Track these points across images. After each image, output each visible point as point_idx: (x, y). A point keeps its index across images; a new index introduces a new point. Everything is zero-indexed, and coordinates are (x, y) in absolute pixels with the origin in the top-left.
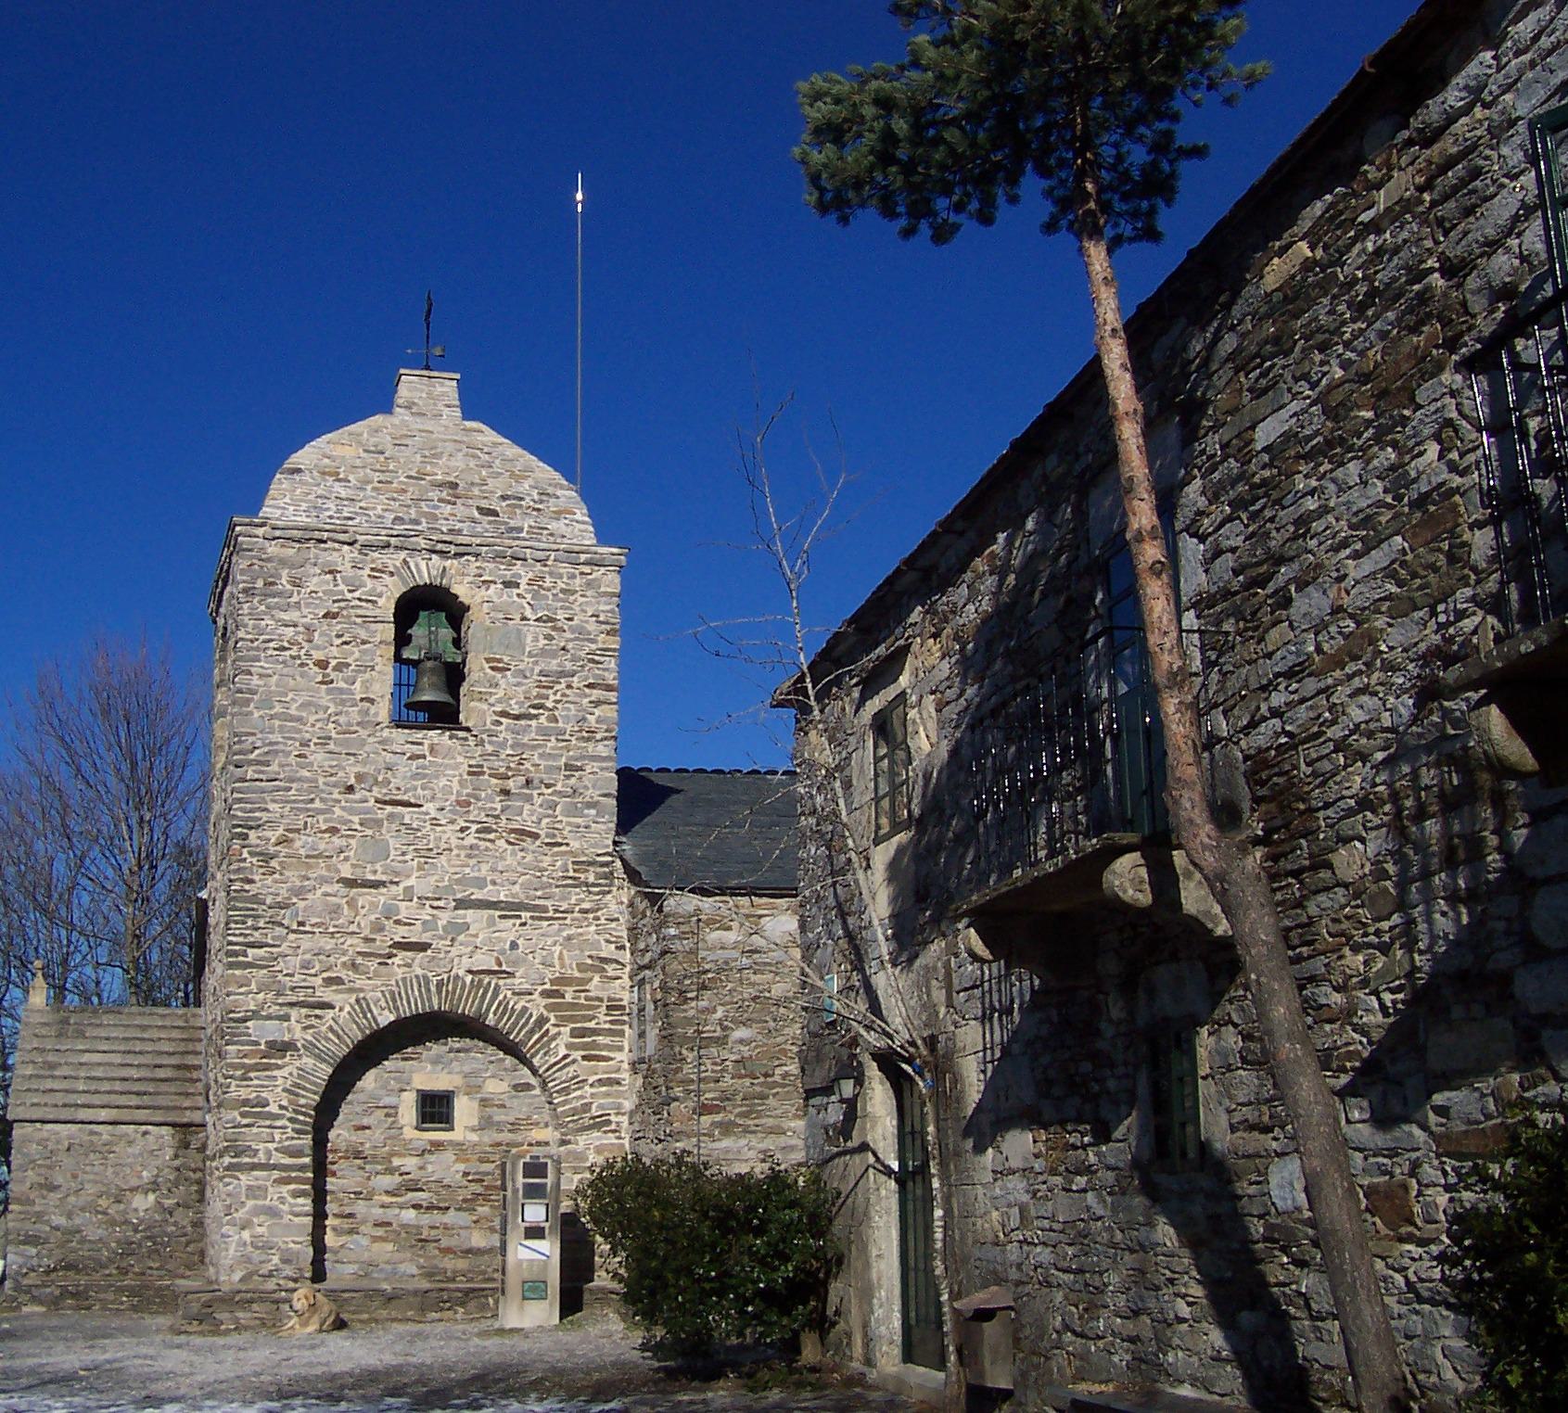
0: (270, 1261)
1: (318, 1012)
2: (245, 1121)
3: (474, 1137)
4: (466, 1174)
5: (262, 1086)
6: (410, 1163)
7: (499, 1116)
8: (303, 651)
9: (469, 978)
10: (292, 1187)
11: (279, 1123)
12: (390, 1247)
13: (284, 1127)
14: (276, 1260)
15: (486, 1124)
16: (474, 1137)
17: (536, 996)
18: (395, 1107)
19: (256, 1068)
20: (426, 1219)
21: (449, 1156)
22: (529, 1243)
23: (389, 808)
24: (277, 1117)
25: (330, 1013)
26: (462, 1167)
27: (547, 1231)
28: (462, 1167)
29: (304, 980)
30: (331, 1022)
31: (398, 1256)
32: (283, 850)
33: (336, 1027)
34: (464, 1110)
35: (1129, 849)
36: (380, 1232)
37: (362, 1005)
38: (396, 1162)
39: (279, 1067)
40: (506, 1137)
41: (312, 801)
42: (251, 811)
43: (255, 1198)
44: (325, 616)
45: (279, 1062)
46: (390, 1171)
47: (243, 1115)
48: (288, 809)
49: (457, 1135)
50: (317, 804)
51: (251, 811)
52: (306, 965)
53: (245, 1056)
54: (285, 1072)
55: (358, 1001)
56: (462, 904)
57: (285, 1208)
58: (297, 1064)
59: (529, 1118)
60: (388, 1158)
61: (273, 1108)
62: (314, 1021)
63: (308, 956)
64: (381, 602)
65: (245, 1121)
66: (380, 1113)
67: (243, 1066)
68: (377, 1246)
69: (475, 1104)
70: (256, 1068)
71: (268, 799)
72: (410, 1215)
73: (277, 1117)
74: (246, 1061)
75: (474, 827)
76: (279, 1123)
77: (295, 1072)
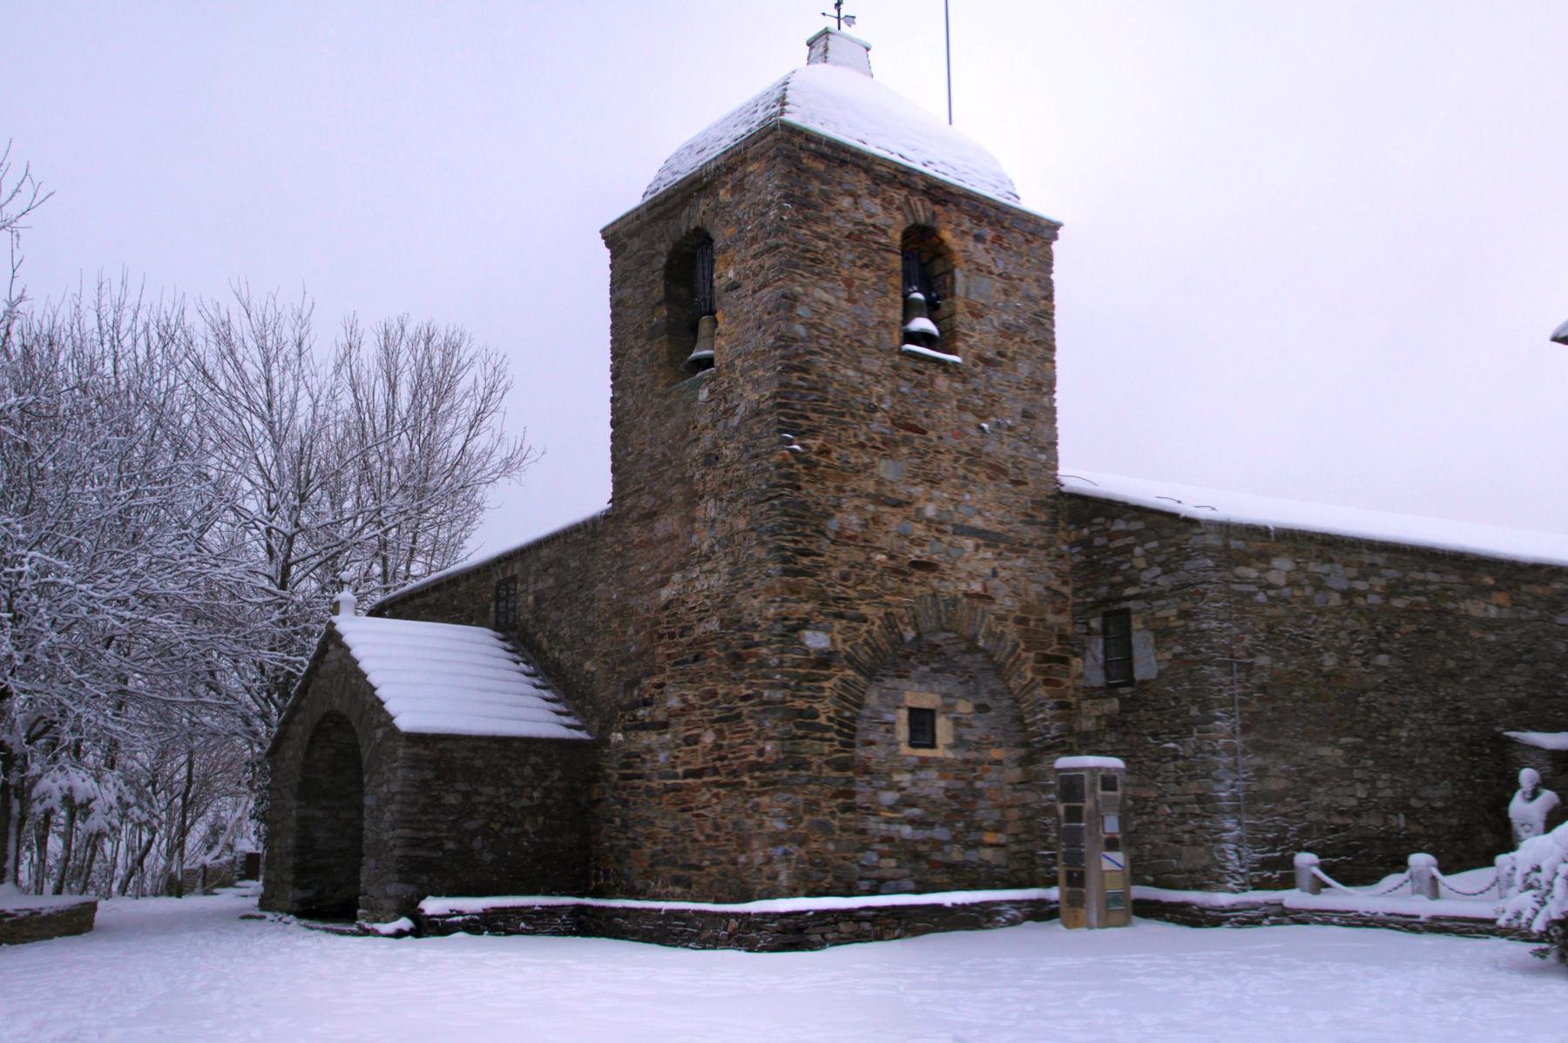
0: (825, 878)
1: (854, 624)
2: (800, 733)
3: (950, 755)
4: (947, 790)
5: (813, 697)
6: (904, 779)
7: (969, 736)
8: (833, 267)
9: (965, 600)
10: (840, 801)
11: (828, 735)
12: (893, 863)
13: (832, 740)
14: (830, 879)
15: (959, 743)
16: (950, 755)
17: (1010, 622)
18: (893, 723)
19: (807, 678)
20: (921, 834)
21: (932, 774)
22: (1109, 854)
23: (903, 432)
24: (827, 729)
25: (864, 627)
26: (942, 783)
27: (1120, 843)
28: (942, 783)
29: (844, 592)
30: (866, 635)
31: (901, 872)
32: (824, 461)
33: (870, 641)
34: (943, 729)
35: (1097, 547)
36: (885, 847)
37: (890, 620)
38: (896, 778)
39: (827, 678)
40: (972, 755)
41: (843, 415)
42: (794, 417)
43: (811, 812)
44: (848, 237)
45: (826, 672)
46: (892, 786)
47: (798, 726)
48: (826, 419)
49: (938, 753)
50: (847, 419)
51: (794, 417)
52: (845, 577)
53: (799, 666)
54: (834, 681)
55: (887, 614)
56: (962, 530)
57: (836, 823)
58: (840, 674)
59: (988, 738)
60: (889, 774)
61: (823, 720)
62: (852, 634)
63: (846, 568)
64: (890, 232)
65: (800, 733)
66: (882, 729)
67: (796, 676)
68: (884, 862)
69: (950, 723)
70: (807, 678)
71: (808, 407)
72: (907, 831)
73: (827, 729)
74: (800, 670)
75: (964, 459)
76: (828, 735)
77: (839, 683)
